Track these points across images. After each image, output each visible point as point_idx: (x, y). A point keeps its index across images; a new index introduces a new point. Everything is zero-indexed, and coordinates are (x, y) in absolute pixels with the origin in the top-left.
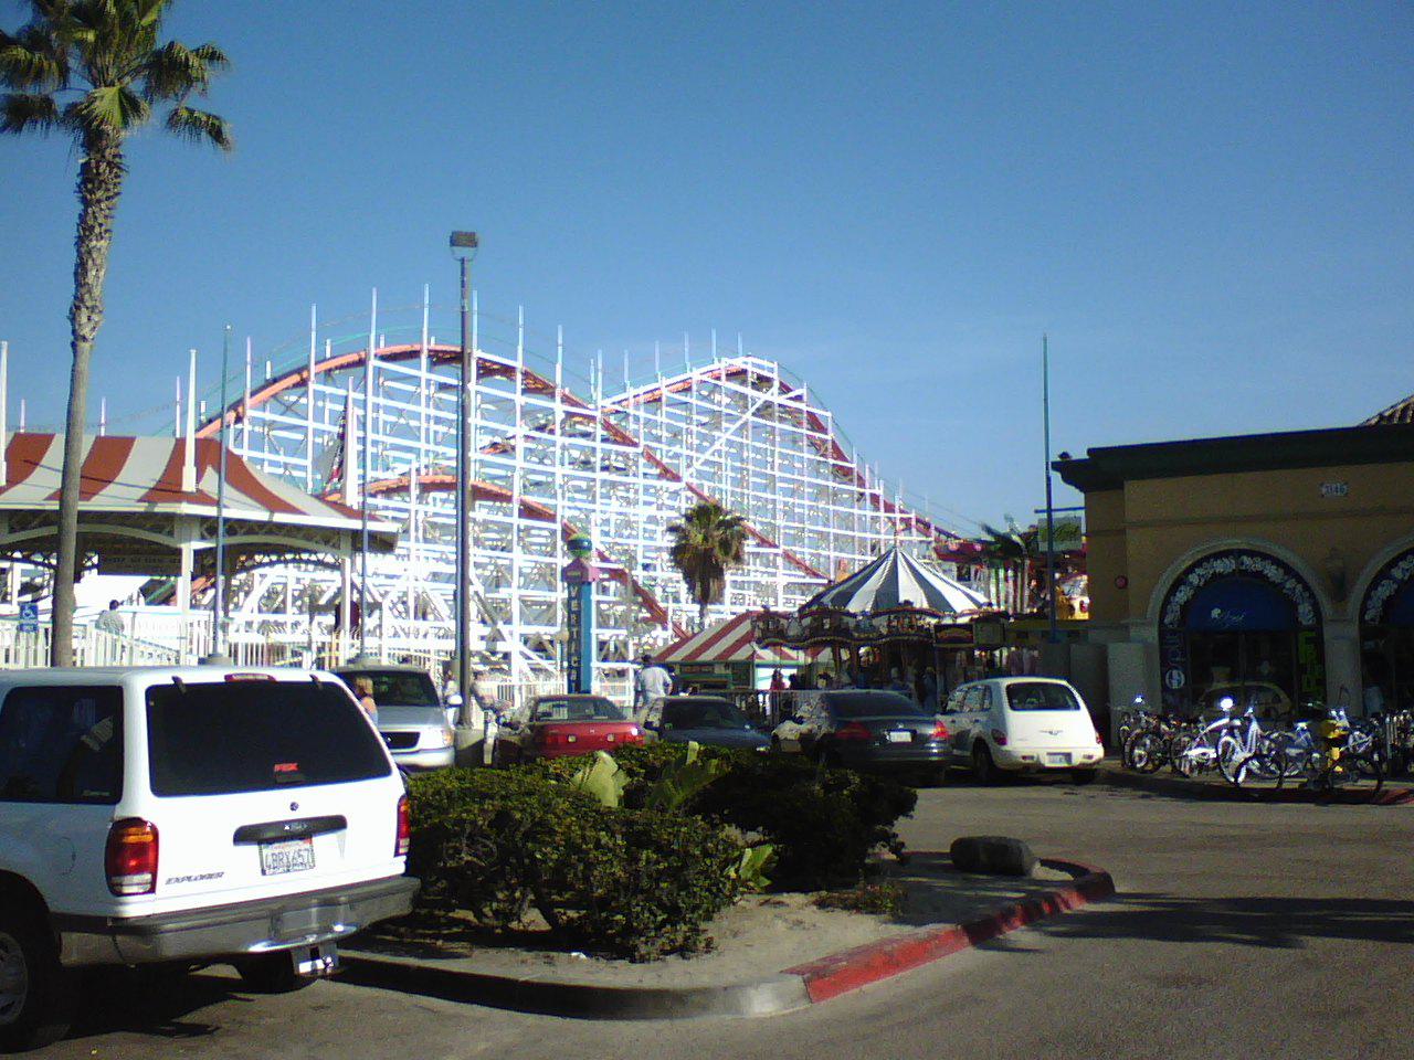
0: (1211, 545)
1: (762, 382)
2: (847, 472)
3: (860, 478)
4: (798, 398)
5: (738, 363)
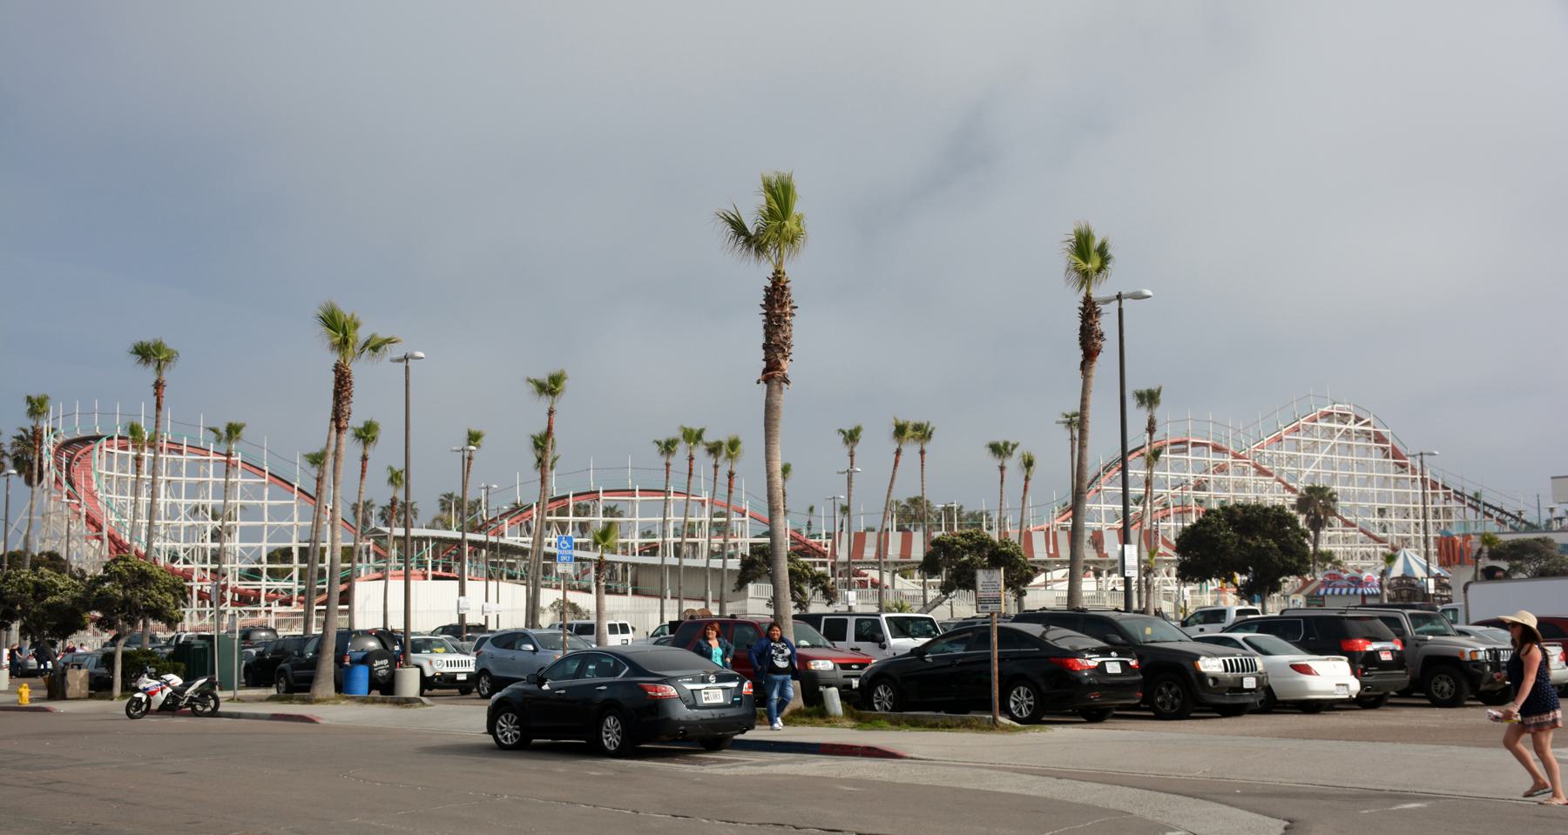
1: (1344, 418)
2: (1403, 466)
3: (1413, 468)
4: (1368, 424)
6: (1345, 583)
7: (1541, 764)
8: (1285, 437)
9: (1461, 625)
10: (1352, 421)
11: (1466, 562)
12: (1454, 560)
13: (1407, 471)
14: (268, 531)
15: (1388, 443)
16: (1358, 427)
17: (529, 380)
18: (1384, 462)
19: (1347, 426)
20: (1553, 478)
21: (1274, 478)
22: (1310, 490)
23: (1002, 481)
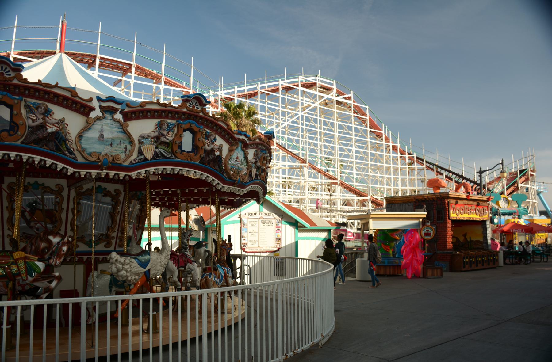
0: (17, 216)
4: (349, 98)
9: (139, 340)
13: (382, 139)
14: (371, 182)
15: (367, 116)
17: (75, 85)
19: (329, 96)
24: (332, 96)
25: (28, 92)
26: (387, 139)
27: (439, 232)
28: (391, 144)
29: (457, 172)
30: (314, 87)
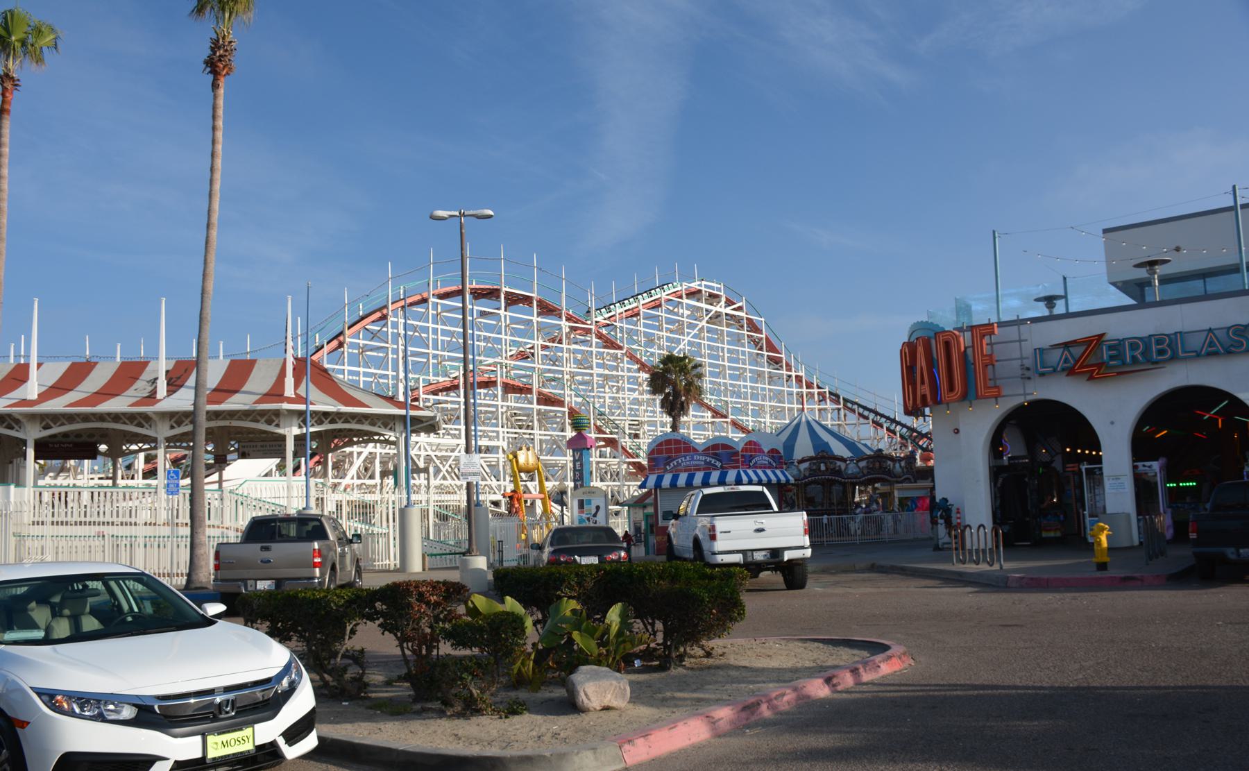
1: (713, 298)
3: (787, 365)
4: (740, 309)
5: (695, 285)
6: (700, 460)
7: (218, 102)
8: (642, 310)
10: (723, 303)
11: (981, 391)
12: (951, 388)
13: (781, 366)
15: (762, 334)
16: (729, 310)
18: (758, 354)
19: (718, 309)
20: (1105, 231)
21: (624, 351)
22: (669, 360)
23: (725, 532)
24: (721, 307)
25: (877, 482)
26: (789, 368)
27: (108, 478)
28: (793, 374)
29: (887, 414)
30: (698, 296)
